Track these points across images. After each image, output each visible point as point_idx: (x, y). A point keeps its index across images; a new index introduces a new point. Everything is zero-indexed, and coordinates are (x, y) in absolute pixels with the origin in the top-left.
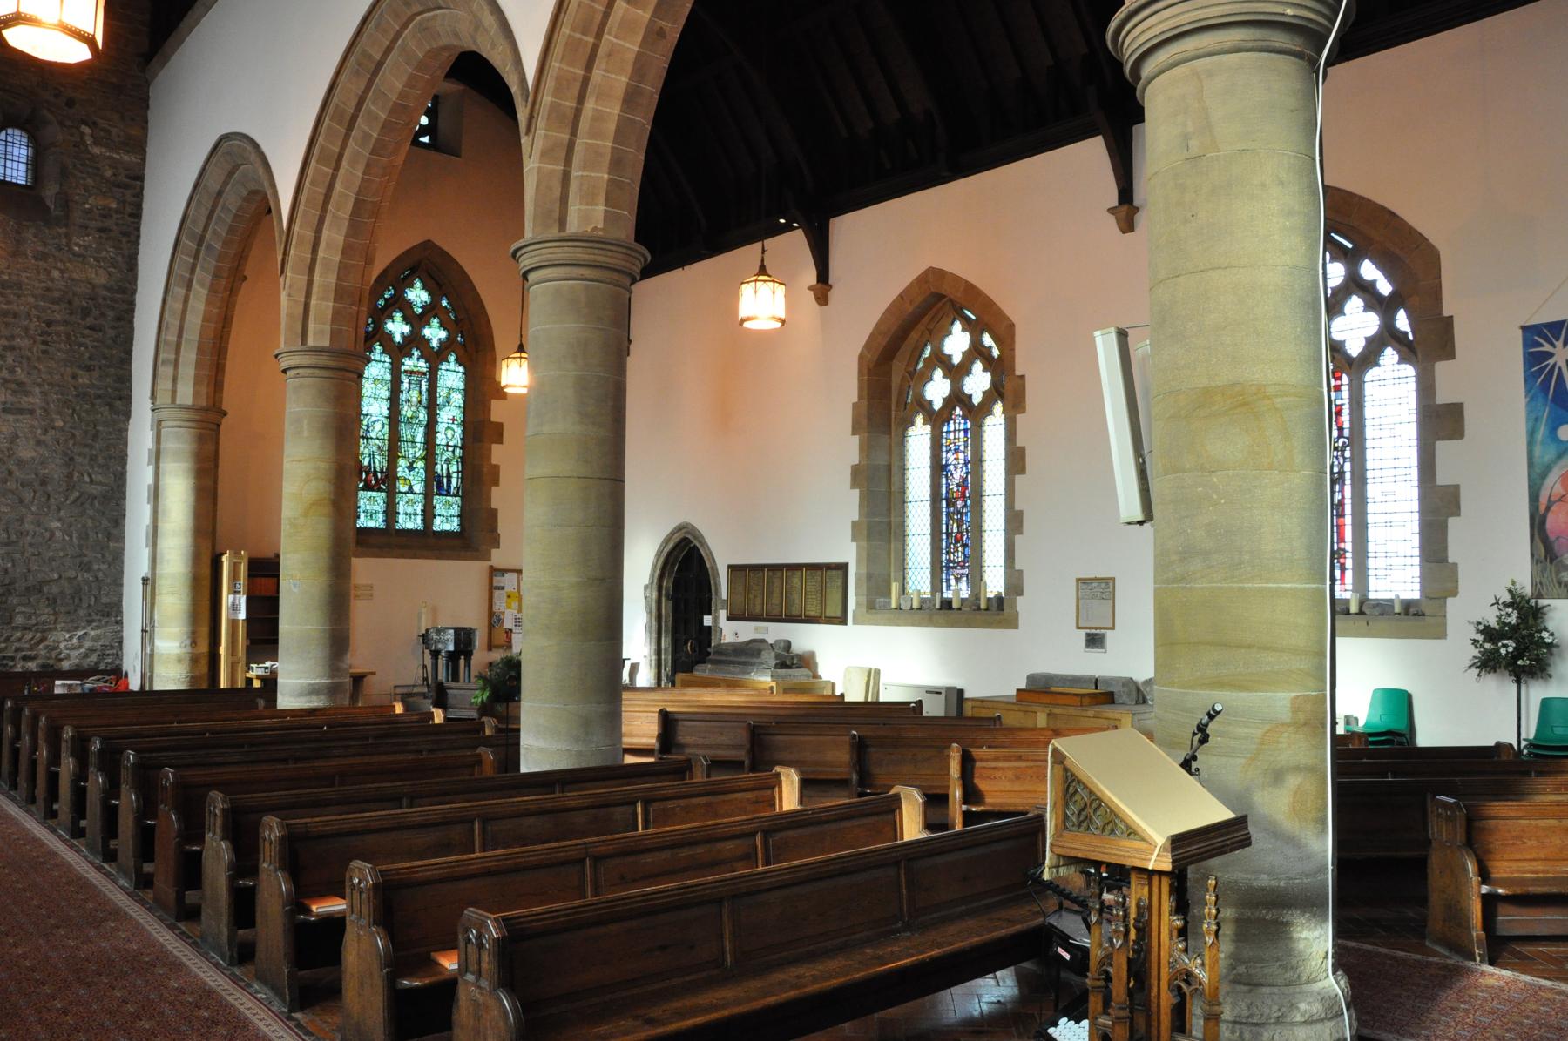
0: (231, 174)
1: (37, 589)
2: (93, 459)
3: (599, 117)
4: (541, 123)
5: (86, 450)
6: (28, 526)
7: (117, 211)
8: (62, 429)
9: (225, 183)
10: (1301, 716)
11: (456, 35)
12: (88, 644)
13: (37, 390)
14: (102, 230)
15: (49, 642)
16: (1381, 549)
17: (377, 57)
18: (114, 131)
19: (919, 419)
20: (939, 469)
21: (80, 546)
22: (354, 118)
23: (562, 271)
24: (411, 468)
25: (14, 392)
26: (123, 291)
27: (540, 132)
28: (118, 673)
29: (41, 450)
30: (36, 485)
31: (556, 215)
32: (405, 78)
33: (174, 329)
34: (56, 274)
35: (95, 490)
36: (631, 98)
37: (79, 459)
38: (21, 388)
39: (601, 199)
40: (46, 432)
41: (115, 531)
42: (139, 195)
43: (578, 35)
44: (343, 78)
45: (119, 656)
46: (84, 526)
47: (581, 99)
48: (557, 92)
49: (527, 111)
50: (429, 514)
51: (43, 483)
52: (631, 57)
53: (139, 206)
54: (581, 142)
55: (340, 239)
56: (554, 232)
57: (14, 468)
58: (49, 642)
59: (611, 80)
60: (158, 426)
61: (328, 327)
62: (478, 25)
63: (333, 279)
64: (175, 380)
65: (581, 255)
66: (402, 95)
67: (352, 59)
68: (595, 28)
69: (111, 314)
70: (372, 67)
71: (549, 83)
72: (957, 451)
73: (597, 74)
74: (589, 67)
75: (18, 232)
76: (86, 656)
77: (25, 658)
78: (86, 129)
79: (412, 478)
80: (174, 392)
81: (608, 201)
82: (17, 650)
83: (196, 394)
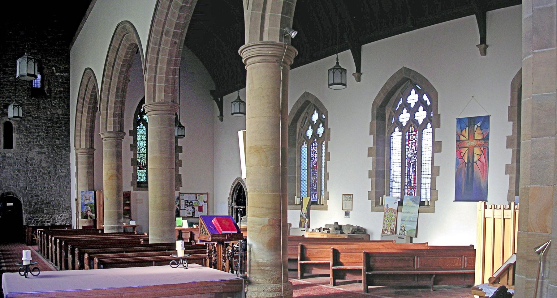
1: (49, 203)
2: (61, 165)
3: (161, 69)
6: (46, 186)
8: (53, 157)
9: (88, 82)
10: (271, 223)
12: (63, 218)
15: (53, 217)
16: (424, 186)
18: (61, 67)
19: (397, 129)
20: (310, 159)
23: (154, 112)
26: (66, 115)
28: (70, 226)
29: (48, 164)
34: (49, 112)
35: (62, 174)
37: (58, 166)
38: (42, 147)
41: (68, 186)
44: (110, 53)
45: (71, 221)
47: (157, 64)
48: (151, 62)
51: (49, 173)
52: (168, 51)
54: (158, 75)
57: (41, 169)
58: (53, 217)
59: (164, 58)
60: (77, 154)
65: (158, 108)
66: (125, 57)
69: (63, 122)
72: (315, 153)
74: (158, 54)
75: (38, 102)
77: (47, 222)
78: (54, 68)
82: (46, 220)
83: (86, 144)
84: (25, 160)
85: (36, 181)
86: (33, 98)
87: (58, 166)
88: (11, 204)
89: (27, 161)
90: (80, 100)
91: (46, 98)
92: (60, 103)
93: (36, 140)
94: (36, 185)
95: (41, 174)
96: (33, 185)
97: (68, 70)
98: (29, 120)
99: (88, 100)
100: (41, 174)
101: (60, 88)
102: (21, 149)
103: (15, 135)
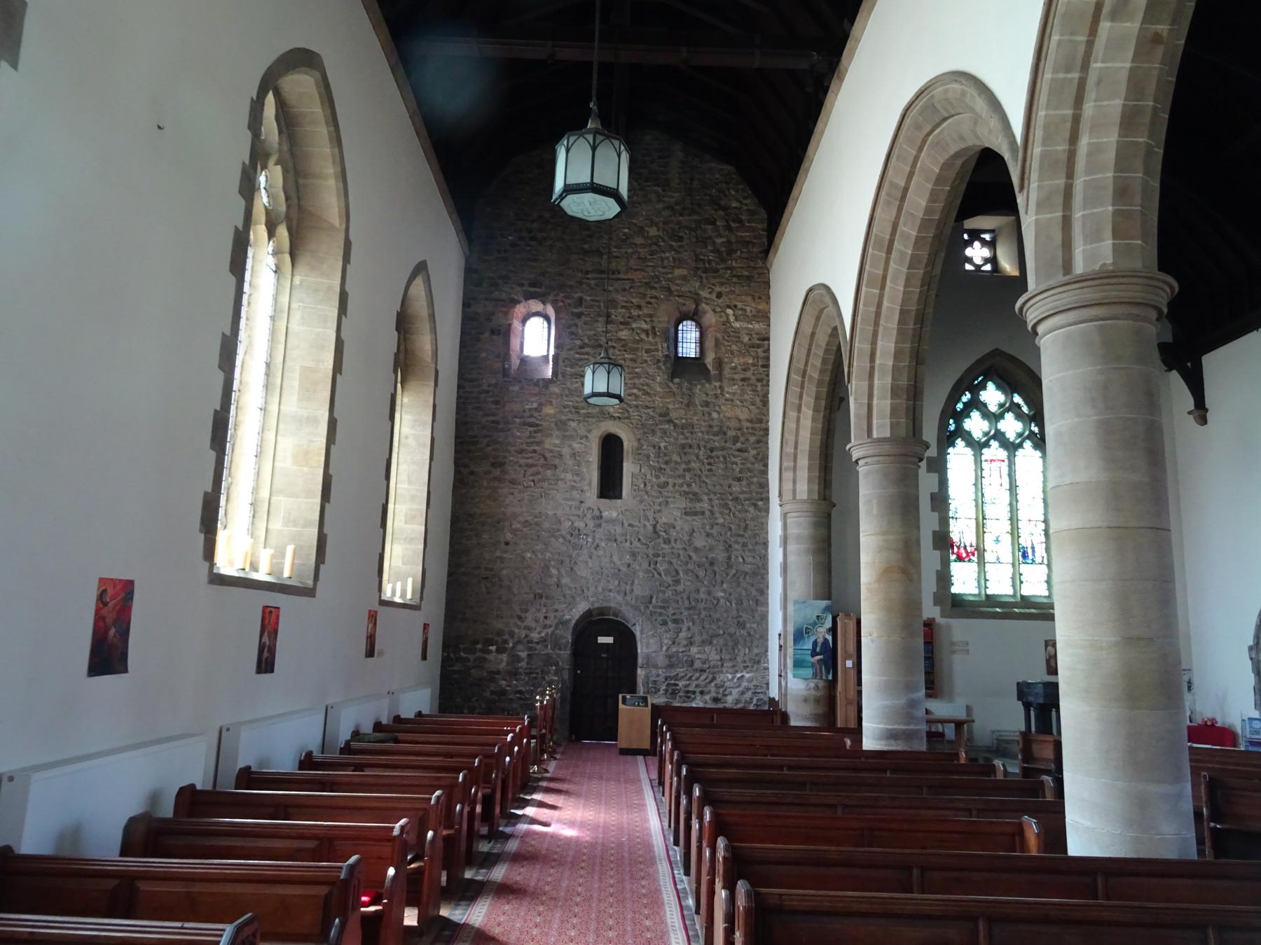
0: (818, 318)
2: (744, 545)
3: (1095, 150)
4: (1034, 176)
5: (740, 540)
7: (753, 365)
9: (816, 326)
11: (962, 138)
12: (745, 684)
13: (706, 498)
14: (743, 380)
15: (718, 681)
17: (903, 184)
18: (748, 309)
21: (737, 610)
22: (891, 242)
24: (997, 540)
25: (691, 500)
27: (1034, 185)
30: (707, 565)
31: (1060, 261)
32: (927, 194)
33: (791, 444)
35: (747, 568)
36: (1128, 121)
39: (1108, 232)
40: (712, 527)
41: (761, 598)
42: (768, 351)
43: (1061, 76)
44: (878, 210)
46: (740, 595)
47: (1074, 138)
48: (1047, 140)
49: (1019, 167)
50: (1016, 579)
51: (712, 564)
52: (1124, 76)
53: (768, 358)
54: (1079, 182)
55: (891, 346)
56: (1062, 278)
58: (718, 681)
60: (784, 516)
61: (888, 421)
62: (976, 119)
63: (889, 380)
64: (794, 482)
67: (883, 193)
68: (1079, 62)
70: (899, 195)
71: (1038, 133)
73: (1089, 108)
75: (690, 390)
76: (743, 693)
78: (729, 311)
79: (999, 549)
80: (794, 491)
81: (1116, 234)
83: (810, 491)
84: (650, 528)
85: (677, 582)
86: (677, 380)
87: (736, 546)
88: (610, 640)
89: (655, 531)
90: (793, 376)
91: (709, 380)
92: (743, 392)
93: (681, 481)
94: (676, 593)
95: (690, 566)
96: (669, 593)
97: (765, 317)
98: (664, 432)
99: (816, 375)
100: (690, 566)
101: (744, 355)
102: (641, 501)
103: (629, 468)
